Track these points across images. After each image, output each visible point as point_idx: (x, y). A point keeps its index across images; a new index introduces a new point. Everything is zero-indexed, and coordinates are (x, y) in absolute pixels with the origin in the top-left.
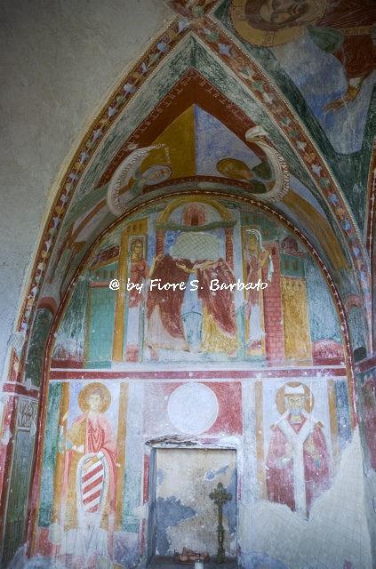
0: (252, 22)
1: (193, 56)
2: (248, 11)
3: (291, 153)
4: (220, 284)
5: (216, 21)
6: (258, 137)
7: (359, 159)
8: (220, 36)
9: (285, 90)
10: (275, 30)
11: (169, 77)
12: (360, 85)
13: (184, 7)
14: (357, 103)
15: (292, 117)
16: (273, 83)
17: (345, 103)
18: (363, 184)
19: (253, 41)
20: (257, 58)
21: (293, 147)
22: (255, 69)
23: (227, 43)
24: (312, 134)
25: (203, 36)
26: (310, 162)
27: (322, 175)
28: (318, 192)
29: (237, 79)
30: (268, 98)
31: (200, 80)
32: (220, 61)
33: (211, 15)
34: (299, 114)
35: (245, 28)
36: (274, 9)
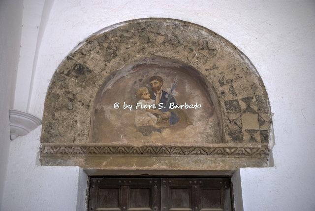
4: (175, 106)
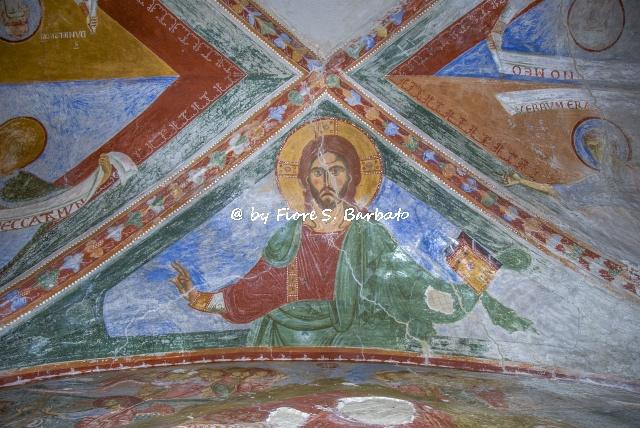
0: (314, 145)
1: (264, 76)
2: (328, 139)
3: (91, 220)
5: (317, 103)
6: (114, 169)
7: (94, 337)
8: (296, 107)
9: (208, 200)
10: (301, 176)
11: (233, 44)
12: (214, 310)
13: (339, 67)
14: (186, 312)
15: (163, 214)
16: (220, 181)
17: (186, 295)
18: (49, 354)
19: (285, 149)
20: (260, 156)
21: (111, 218)
22: (244, 155)
23: (285, 117)
24: (135, 249)
25: (297, 88)
26: (88, 249)
27: (64, 273)
28: (18, 273)
29: (226, 133)
30: (196, 177)
31: (225, 84)
32: (259, 107)
33: (326, 96)
34: (168, 225)
35: (303, 140)
36: (330, 169)
